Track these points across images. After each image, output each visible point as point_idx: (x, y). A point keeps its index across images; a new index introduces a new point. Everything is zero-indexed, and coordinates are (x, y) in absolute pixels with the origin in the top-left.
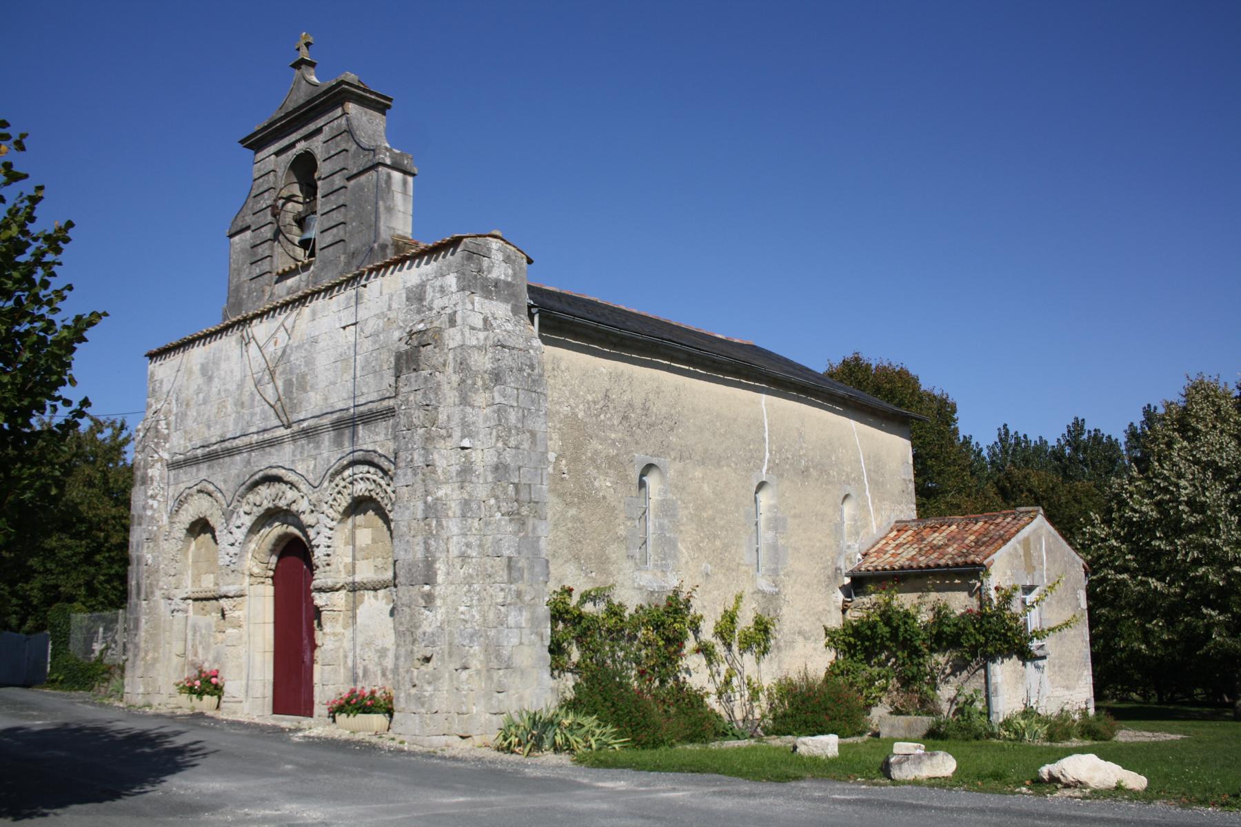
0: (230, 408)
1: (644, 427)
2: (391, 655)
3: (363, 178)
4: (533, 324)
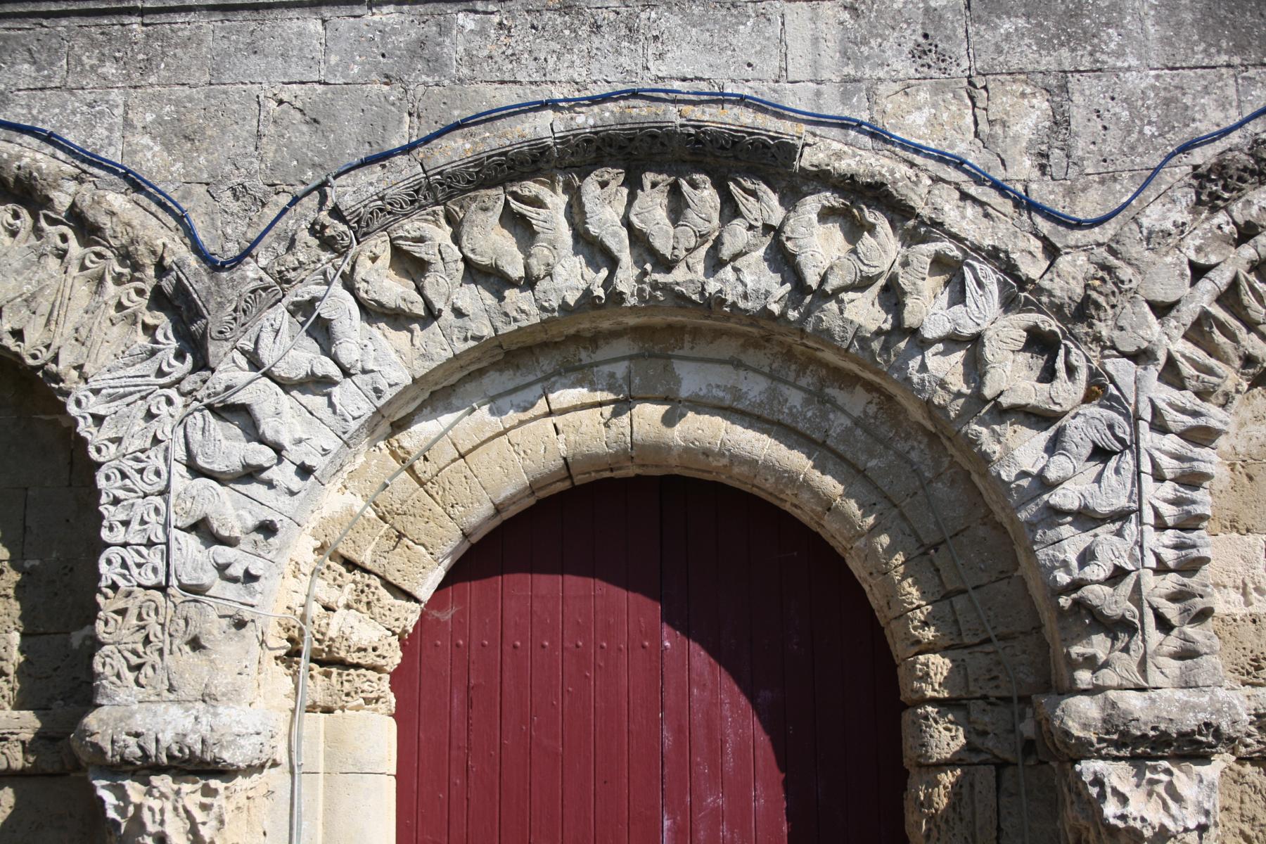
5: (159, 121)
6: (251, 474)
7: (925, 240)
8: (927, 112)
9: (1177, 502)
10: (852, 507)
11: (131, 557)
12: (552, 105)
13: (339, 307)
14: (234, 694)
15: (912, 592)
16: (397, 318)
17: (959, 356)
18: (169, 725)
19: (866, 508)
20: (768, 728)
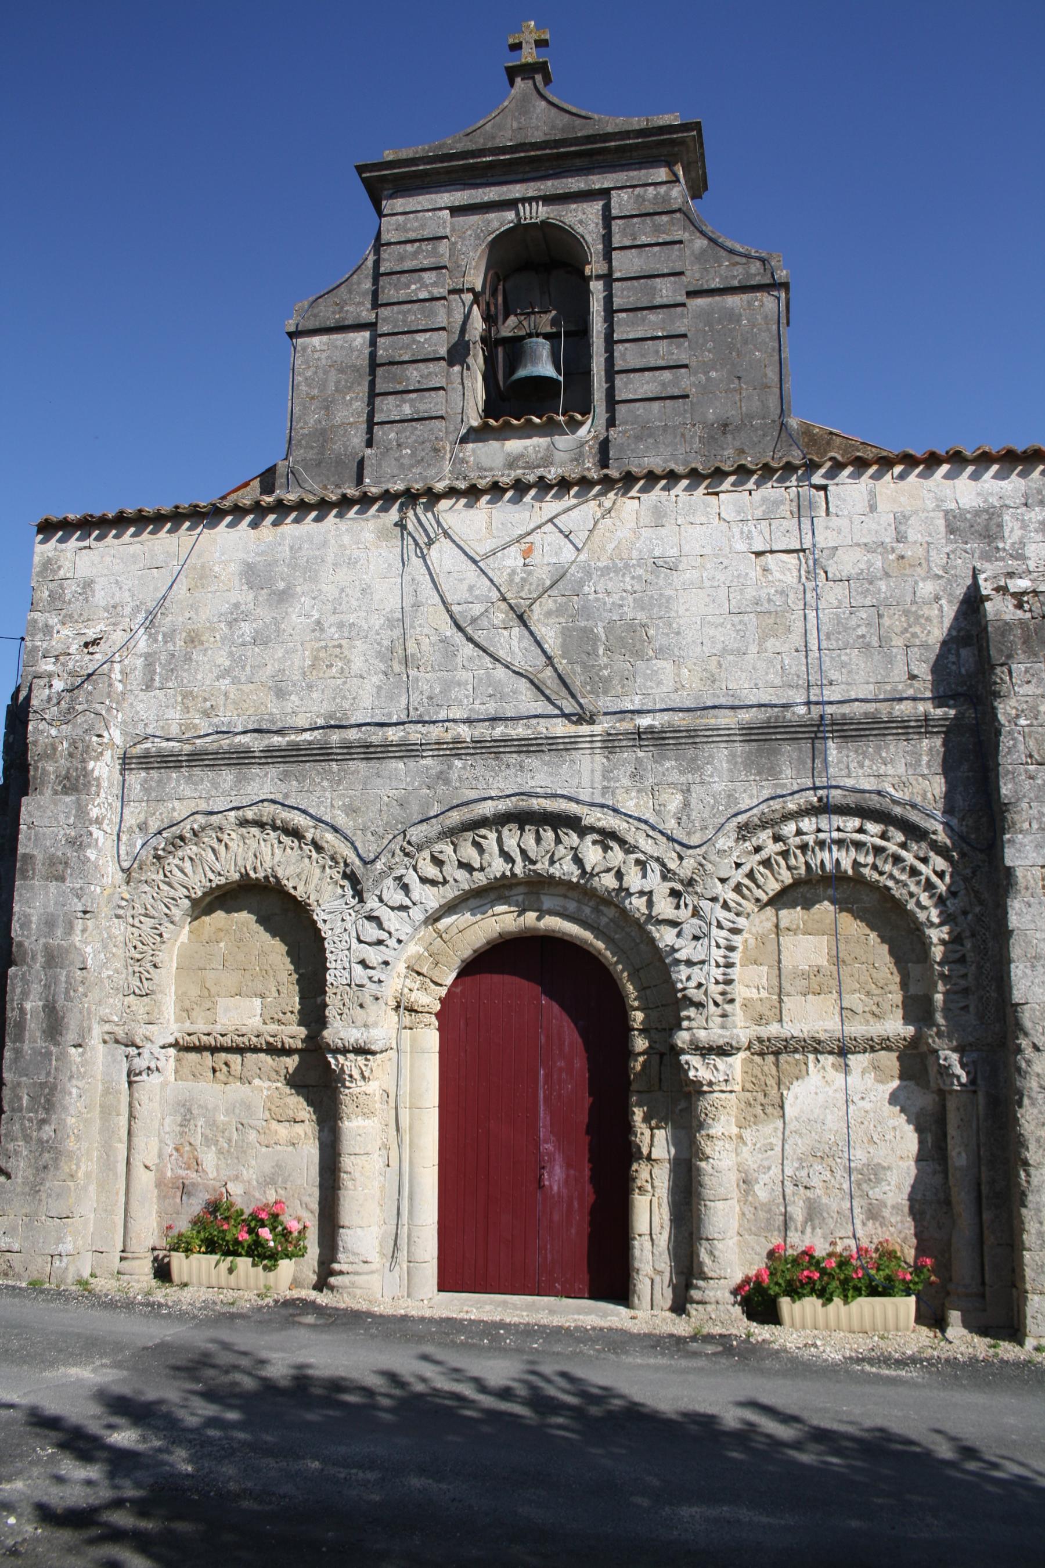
3: (732, 301)
5: (344, 805)
6: (380, 942)
7: (633, 852)
8: (635, 801)
9: (725, 957)
10: (608, 954)
11: (338, 974)
12: (491, 798)
13: (411, 879)
14: (375, 1024)
15: (630, 987)
16: (433, 883)
17: (645, 898)
18: (352, 1036)
19: (614, 954)
20: (581, 1035)
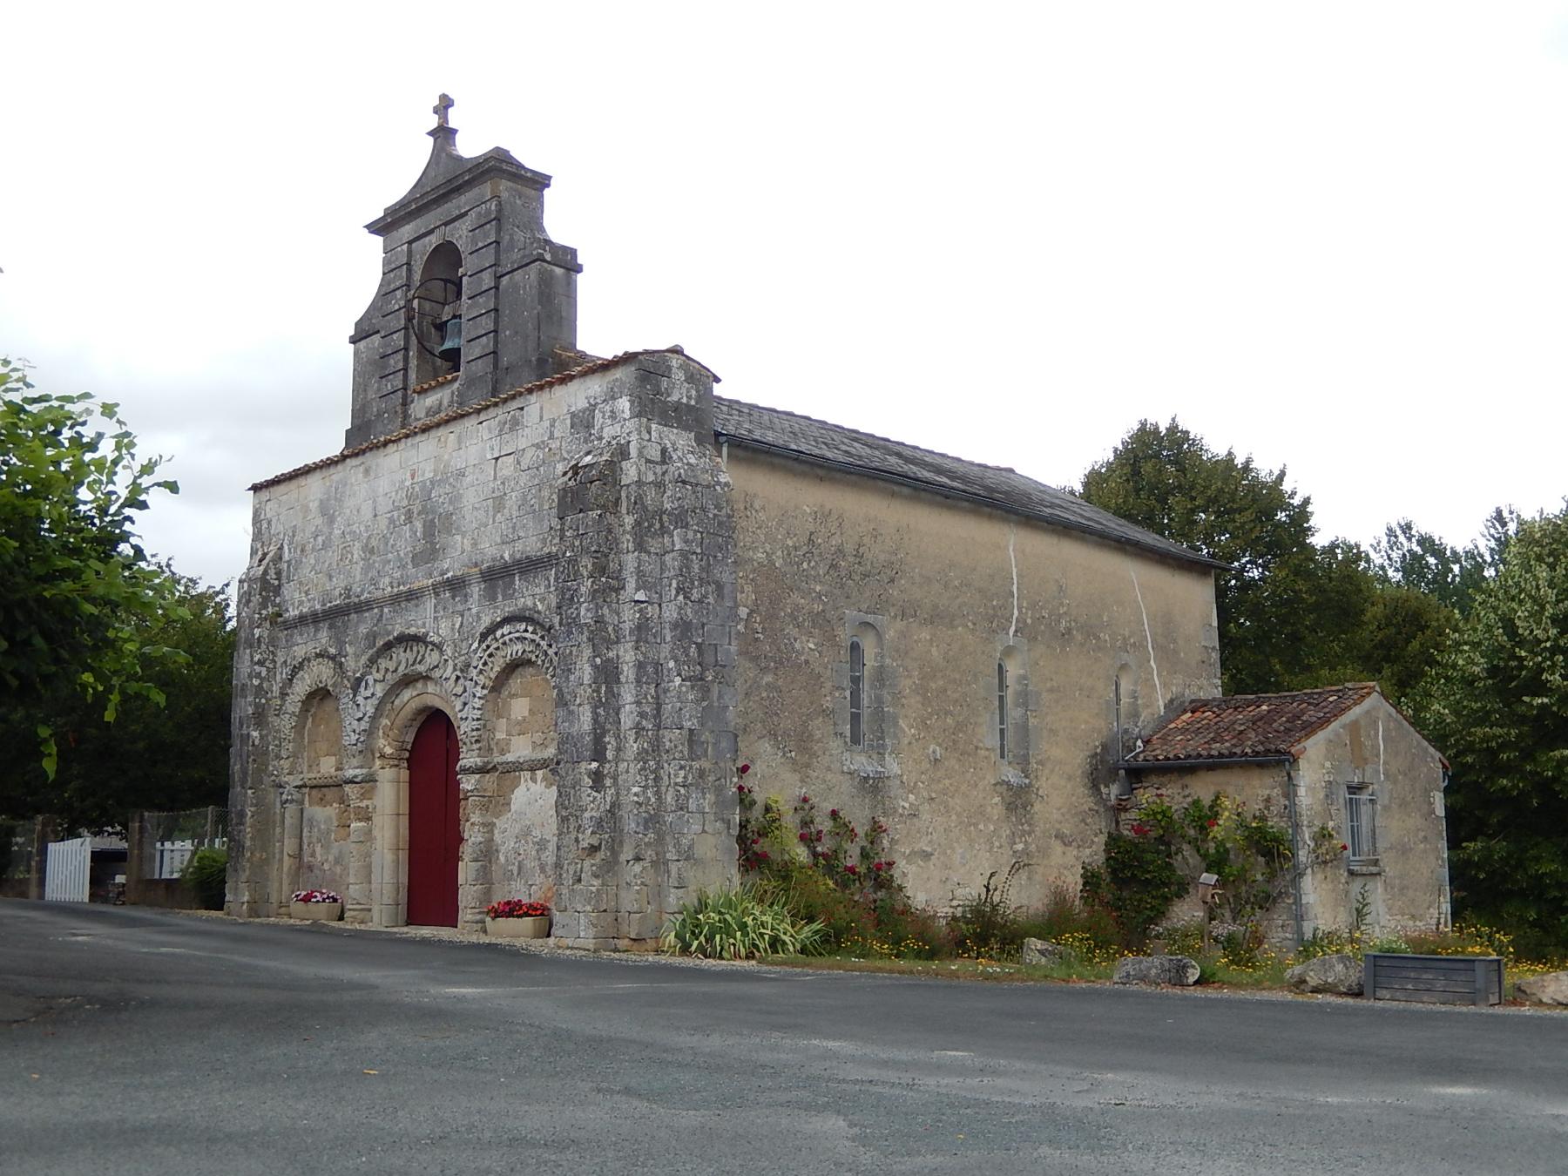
0: (357, 553)
1: (857, 578)
2: (552, 847)
4: (720, 456)
